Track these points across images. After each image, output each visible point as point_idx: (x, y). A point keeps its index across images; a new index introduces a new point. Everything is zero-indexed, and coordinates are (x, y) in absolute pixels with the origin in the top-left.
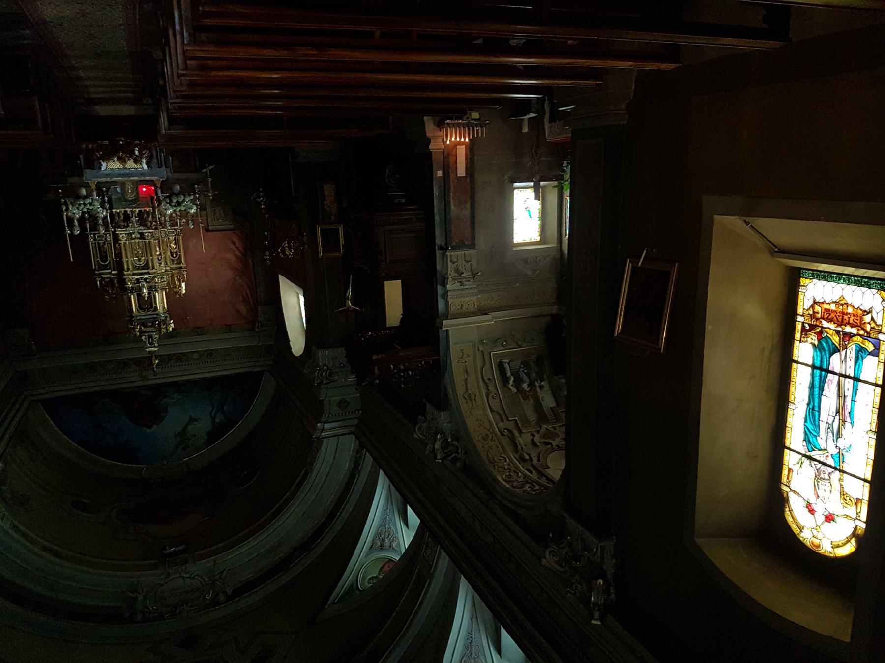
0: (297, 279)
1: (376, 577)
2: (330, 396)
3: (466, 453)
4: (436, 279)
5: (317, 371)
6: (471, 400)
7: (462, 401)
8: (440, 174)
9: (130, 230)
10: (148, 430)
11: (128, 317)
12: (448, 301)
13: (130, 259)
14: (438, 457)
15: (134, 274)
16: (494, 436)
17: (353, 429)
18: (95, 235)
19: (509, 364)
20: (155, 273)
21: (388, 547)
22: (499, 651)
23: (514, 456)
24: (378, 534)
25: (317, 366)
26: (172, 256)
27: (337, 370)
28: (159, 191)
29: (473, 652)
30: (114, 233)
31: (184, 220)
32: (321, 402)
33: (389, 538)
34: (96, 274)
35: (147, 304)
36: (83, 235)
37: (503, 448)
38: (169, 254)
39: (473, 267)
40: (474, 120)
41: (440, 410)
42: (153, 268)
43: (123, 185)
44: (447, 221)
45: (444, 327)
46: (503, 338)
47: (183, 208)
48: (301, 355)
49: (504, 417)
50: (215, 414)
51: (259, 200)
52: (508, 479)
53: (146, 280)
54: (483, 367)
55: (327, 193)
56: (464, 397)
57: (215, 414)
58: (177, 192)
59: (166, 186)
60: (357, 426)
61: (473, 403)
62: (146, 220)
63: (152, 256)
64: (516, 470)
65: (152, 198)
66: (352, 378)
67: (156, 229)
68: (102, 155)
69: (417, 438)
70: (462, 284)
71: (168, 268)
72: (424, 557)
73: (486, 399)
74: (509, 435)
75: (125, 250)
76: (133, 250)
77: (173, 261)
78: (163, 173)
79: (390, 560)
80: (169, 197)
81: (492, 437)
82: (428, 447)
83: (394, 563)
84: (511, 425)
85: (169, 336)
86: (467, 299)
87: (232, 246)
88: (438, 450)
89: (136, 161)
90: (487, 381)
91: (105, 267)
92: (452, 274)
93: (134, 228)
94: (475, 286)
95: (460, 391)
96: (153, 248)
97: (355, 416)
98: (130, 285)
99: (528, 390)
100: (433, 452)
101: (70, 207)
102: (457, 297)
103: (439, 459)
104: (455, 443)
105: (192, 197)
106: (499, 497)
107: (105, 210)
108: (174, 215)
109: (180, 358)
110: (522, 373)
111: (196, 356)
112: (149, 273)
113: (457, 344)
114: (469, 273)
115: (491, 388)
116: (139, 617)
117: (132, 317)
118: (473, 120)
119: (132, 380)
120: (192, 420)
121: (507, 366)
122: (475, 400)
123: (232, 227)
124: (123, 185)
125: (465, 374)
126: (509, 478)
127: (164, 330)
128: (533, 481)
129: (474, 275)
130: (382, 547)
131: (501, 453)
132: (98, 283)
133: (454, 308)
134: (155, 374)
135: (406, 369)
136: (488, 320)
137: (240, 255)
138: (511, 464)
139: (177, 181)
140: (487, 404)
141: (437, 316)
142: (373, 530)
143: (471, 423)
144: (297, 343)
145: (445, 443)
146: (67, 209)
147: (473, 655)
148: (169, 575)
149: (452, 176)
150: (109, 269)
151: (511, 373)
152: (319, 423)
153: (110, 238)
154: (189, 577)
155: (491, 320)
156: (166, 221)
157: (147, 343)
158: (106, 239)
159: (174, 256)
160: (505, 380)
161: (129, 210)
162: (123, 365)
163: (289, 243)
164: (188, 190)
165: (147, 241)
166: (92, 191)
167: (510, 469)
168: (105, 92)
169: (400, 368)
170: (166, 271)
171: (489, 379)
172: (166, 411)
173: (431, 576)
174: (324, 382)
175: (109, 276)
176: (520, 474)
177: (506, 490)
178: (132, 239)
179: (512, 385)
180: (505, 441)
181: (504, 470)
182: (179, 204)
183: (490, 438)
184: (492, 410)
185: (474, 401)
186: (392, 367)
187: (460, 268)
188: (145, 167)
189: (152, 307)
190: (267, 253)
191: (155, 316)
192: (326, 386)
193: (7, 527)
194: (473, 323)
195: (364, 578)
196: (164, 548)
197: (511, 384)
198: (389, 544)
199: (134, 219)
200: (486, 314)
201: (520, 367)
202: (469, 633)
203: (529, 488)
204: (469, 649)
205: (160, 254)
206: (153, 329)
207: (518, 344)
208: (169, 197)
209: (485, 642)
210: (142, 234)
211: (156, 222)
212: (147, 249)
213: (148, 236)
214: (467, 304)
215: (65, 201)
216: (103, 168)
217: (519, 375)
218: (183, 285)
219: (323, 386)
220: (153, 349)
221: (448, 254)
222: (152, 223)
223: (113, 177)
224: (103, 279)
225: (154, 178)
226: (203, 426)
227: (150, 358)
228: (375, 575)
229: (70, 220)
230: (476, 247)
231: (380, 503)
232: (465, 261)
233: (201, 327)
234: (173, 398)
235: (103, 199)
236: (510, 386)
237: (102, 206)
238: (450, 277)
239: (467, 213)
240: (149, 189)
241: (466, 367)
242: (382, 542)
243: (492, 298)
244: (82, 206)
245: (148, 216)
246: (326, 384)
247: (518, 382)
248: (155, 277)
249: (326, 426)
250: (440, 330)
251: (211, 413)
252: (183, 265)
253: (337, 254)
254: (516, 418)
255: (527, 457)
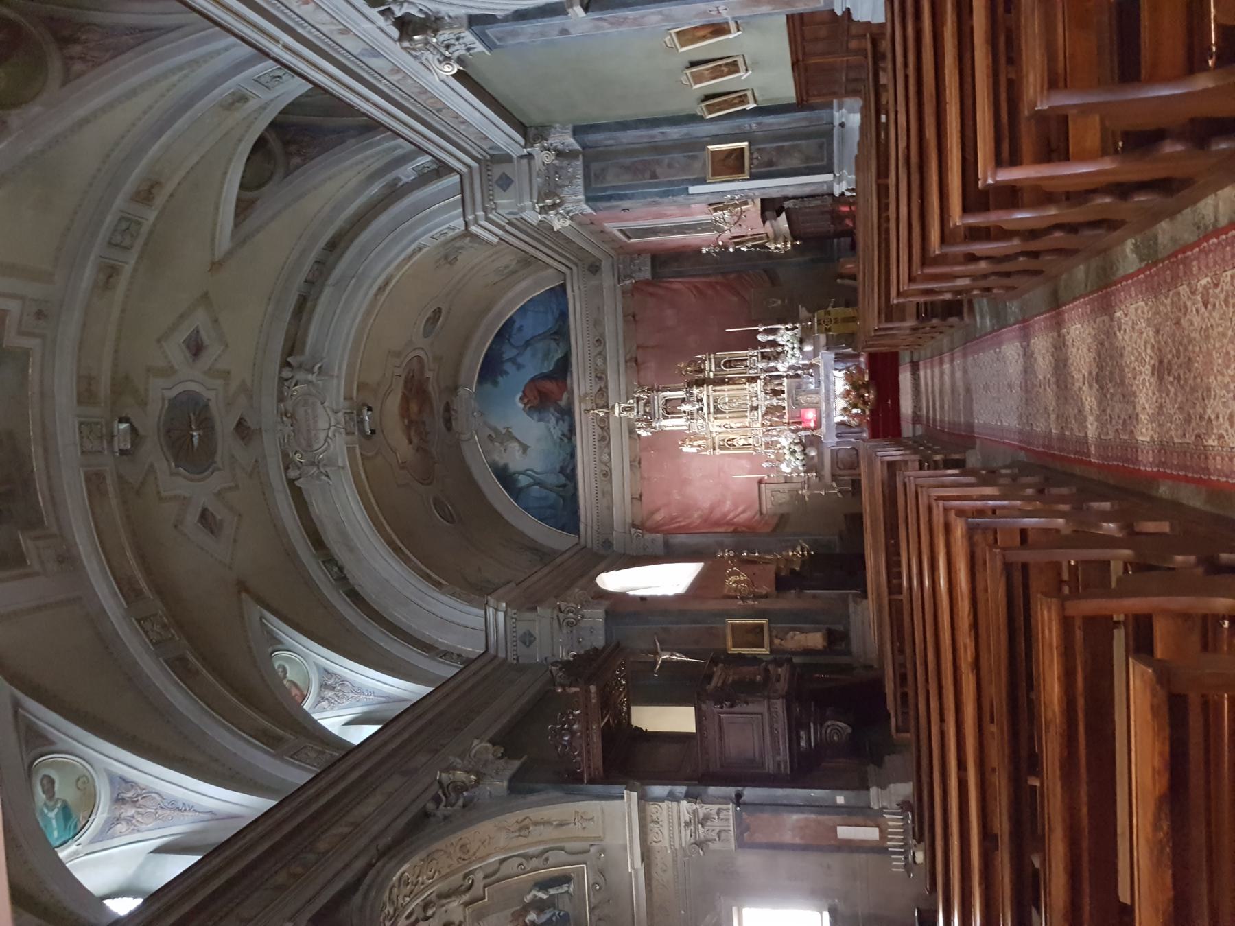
0: (698, 585)
1: (285, 677)
2: (541, 622)
3: (446, 818)
4: (695, 785)
5: (575, 606)
6: (520, 829)
7: (520, 815)
8: (840, 800)
9: (762, 396)
10: (518, 397)
11: (658, 387)
12: (663, 801)
13: (726, 393)
14: (444, 775)
15: (708, 396)
16: (466, 862)
17: (492, 651)
18: (757, 356)
19: (567, 892)
20: (709, 420)
21: (322, 695)
22: (159, 850)
23: (431, 893)
24: (343, 682)
25: (582, 606)
26: (729, 440)
27: (574, 632)
28: (808, 433)
29: (165, 812)
30: (758, 378)
31: (772, 457)
32: (535, 609)
33: (334, 697)
34: (710, 355)
35: (670, 409)
36: (756, 344)
37: (446, 876)
38: (732, 437)
39: (710, 843)
40: (914, 857)
41: (510, 781)
42: (715, 418)
43: (817, 392)
44: (777, 806)
45: (627, 794)
46: (606, 884)
47: (787, 457)
48: (597, 584)
49: (488, 880)
50: (529, 476)
51: (799, 549)
52: (403, 880)
53: (701, 409)
54: (566, 852)
55: (811, 636)
56: (524, 819)
57: (529, 476)
58: (807, 451)
59: (814, 441)
60: (496, 657)
61: (515, 832)
62: (773, 414)
63: (730, 418)
64: (414, 894)
65: (800, 423)
66: (563, 654)
67: (763, 425)
68: (851, 372)
69: (472, 744)
70: (687, 824)
71: (714, 435)
72: (305, 747)
73: (516, 853)
74: (463, 887)
75: (738, 389)
76: (737, 397)
77: (723, 440)
78: (830, 440)
79: (304, 698)
80: (800, 443)
81: (464, 860)
82: (459, 761)
83: (300, 701)
84: (477, 890)
85: (632, 431)
86: (666, 832)
87: (741, 509)
88: (454, 775)
89: (845, 409)
90: (546, 855)
91: (718, 365)
92: (703, 809)
93: (764, 401)
94: (683, 845)
95: (536, 814)
96: (741, 420)
97: (509, 654)
98: (695, 391)
99: (526, 921)
100: (450, 769)
101: (790, 333)
102: (669, 815)
103: (440, 776)
104: (461, 802)
105: (801, 468)
106: (379, 864)
107: (786, 370)
108: (779, 446)
109: (604, 439)
110: (552, 913)
111: (605, 457)
112: (709, 413)
113: (603, 812)
114: (702, 837)
115: (535, 863)
116: (286, 373)
117: (658, 391)
118: (914, 853)
119: (581, 384)
120: (525, 448)
121: (564, 888)
122: (520, 836)
123: (764, 511)
124: (817, 392)
125: (557, 822)
126: (405, 881)
127: (639, 425)
128: (396, 919)
129: (700, 844)
130: (323, 686)
131: (439, 872)
132: (700, 356)
133: (654, 810)
134: (587, 411)
135: (572, 733)
136: (634, 862)
137: (729, 517)
138: (422, 887)
139: (820, 454)
140: (511, 854)
141: (643, 784)
142: (349, 675)
143: (486, 828)
144: (611, 581)
145: (460, 788)
146: (787, 329)
147: (160, 812)
148: (336, 412)
149: (836, 818)
150: (716, 370)
151: (553, 895)
152: (507, 605)
153: (752, 373)
154: (327, 436)
155: (633, 868)
156: (772, 436)
157: (625, 405)
158: (751, 368)
159: (729, 443)
160: (544, 885)
161: (785, 396)
162: (601, 377)
163: (744, 581)
164: (809, 466)
165: (748, 414)
166: (809, 360)
167: (416, 885)
168: (926, 385)
169: (574, 724)
170: (711, 432)
171: (547, 859)
172: (540, 420)
173: (279, 756)
174: (561, 615)
175: (707, 368)
176: (408, 899)
177: (389, 877)
178: (751, 397)
179: (535, 896)
180: (456, 879)
181: (415, 876)
182: (793, 452)
183: (463, 857)
184: (502, 861)
185: (517, 834)
186: (578, 712)
187: (709, 823)
188: (838, 419)
189: (668, 413)
190: (732, 554)
191: (657, 416)
192: (556, 618)
193: (422, 240)
194: (631, 837)
195: (288, 660)
196: (370, 409)
197: (537, 893)
198: (327, 696)
199: (775, 401)
200: (643, 860)
201: (560, 911)
202: (193, 807)
203: (389, 912)
204: (170, 806)
205: (731, 428)
206: (641, 413)
207: (594, 908)
208: (800, 443)
209: (177, 828)
210: (756, 408)
211: (771, 425)
212: (739, 412)
213: (754, 415)
214: (657, 830)
215: (797, 328)
216: (836, 373)
217: (549, 908)
218: (694, 450)
219: (556, 612)
220: (617, 411)
221: (731, 806)
222: (769, 420)
223: (825, 383)
224: (704, 362)
225: (823, 429)
226: (515, 460)
227: (606, 406)
228: (288, 675)
229: (774, 331)
230: (740, 850)
231: (385, 686)
232: (720, 831)
233: (640, 467)
234: (554, 428)
235: (799, 368)
236: (534, 892)
237: (791, 368)
238: (698, 807)
239: (788, 837)
240: (810, 420)
241: (568, 824)
242: (331, 685)
243: (665, 871)
244: (791, 346)
245: (778, 417)
246: (558, 616)
247: (539, 906)
248: (704, 420)
249: (501, 615)
250: (624, 786)
251: (532, 471)
252: (718, 452)
253: (730, 642)
254: (486, 900)
255: (430, 912)
